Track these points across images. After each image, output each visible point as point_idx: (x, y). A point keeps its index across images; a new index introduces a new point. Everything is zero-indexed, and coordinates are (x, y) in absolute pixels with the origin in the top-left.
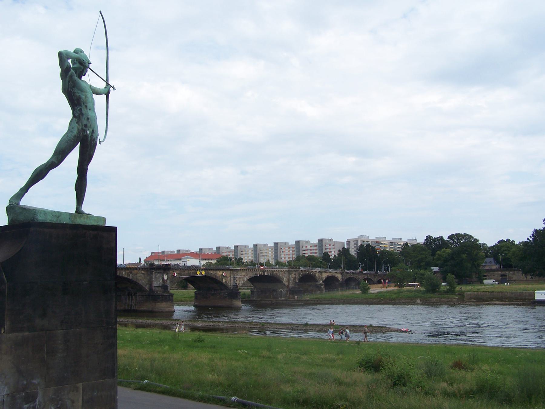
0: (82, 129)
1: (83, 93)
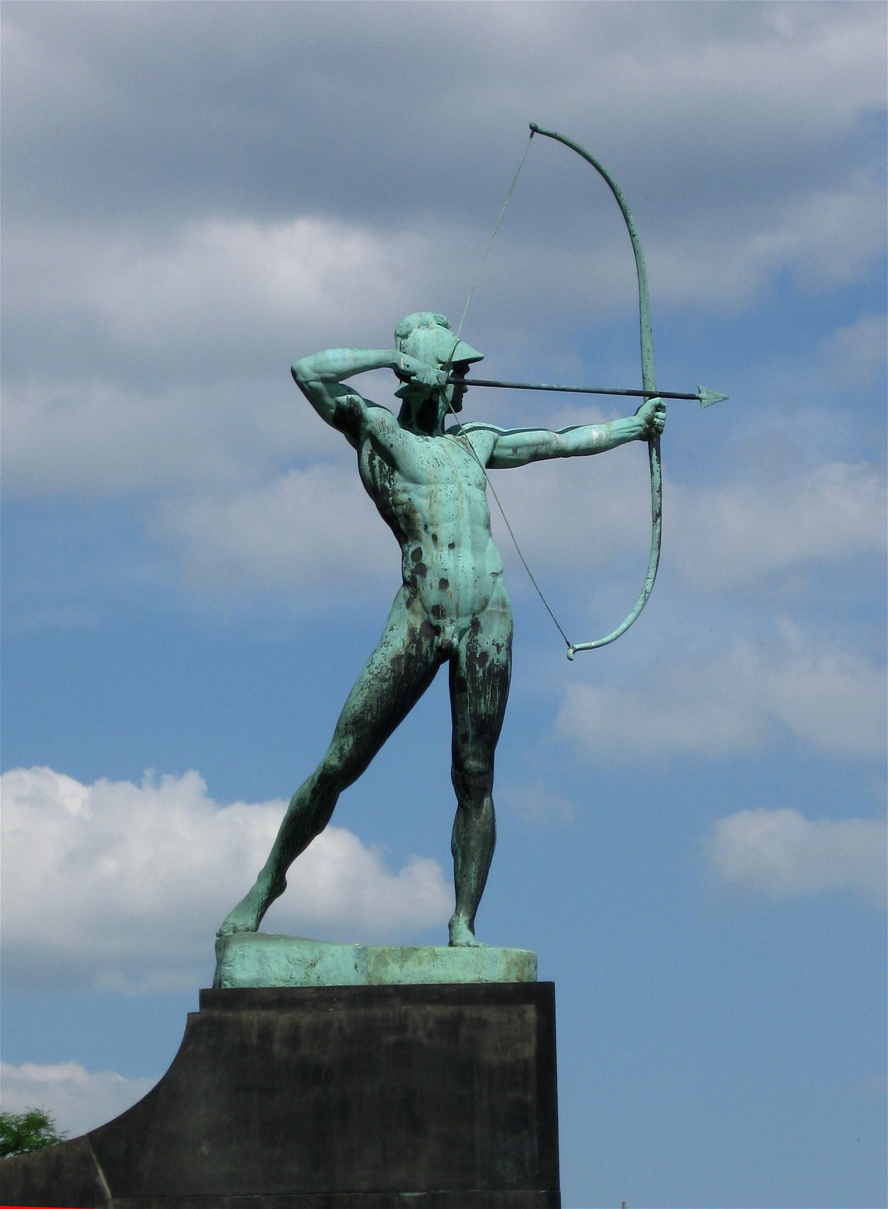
0: (427, 624)
1: (424, 489)
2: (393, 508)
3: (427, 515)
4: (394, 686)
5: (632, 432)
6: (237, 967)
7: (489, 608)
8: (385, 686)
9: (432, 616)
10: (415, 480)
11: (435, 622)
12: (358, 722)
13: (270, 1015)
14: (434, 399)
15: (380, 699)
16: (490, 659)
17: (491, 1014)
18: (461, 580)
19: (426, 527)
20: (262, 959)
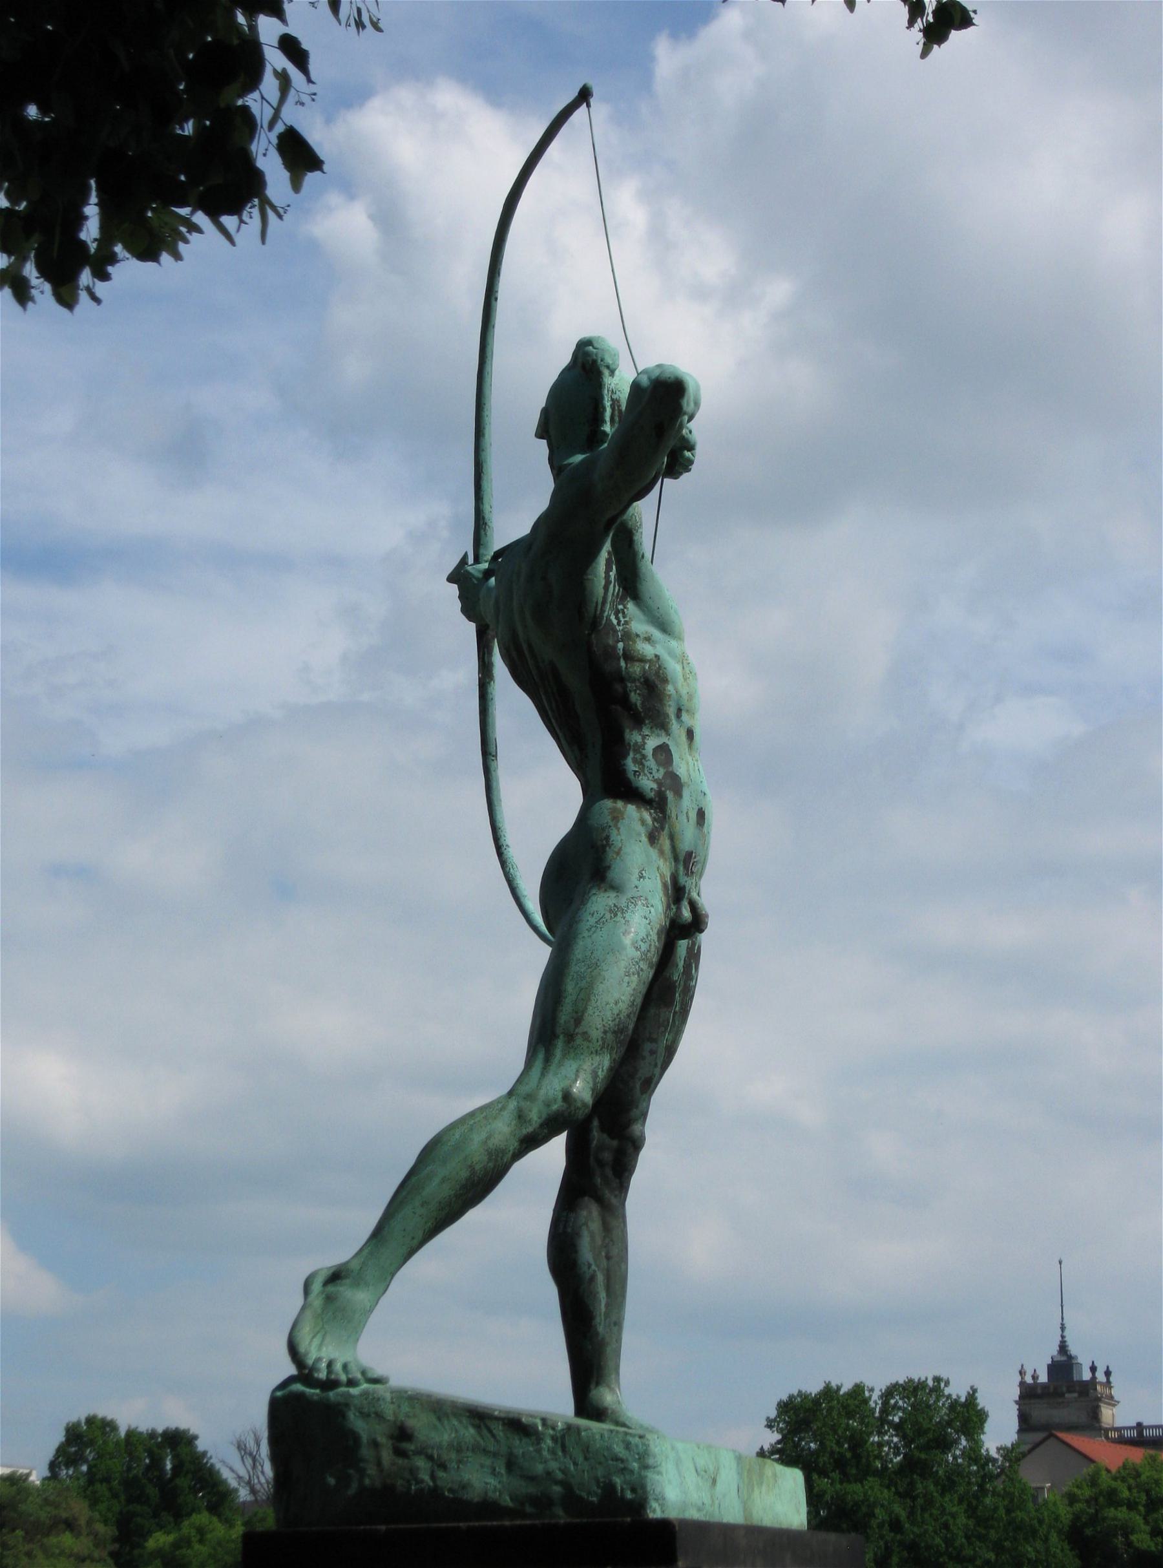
2: (623, 664)
3: (684, 692)
19: (679, 711)
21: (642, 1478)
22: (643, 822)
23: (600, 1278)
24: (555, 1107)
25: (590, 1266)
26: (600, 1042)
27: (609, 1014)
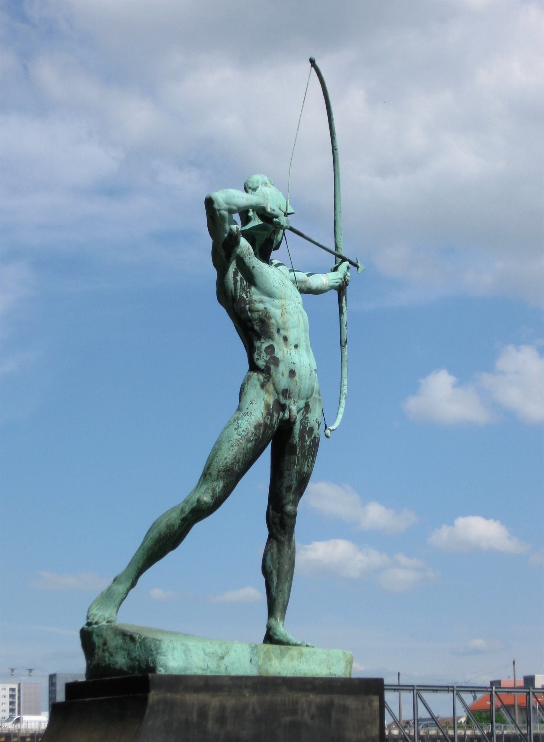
1: (277, 302)
2: (249, 314)
4: (255, 446)
5: (337, 282)
6: (170, 657)
7: (314, 395)
8: (250, 445)
9: (281, 397)
10: (270, 295)
11: (283, 401)
12: (229, 471)
13: (203, 697)
14: (272, 238)
15: (245, 455)
16: (315, 432)
17: (351, 702)
18: (303, 372)
19: (278, 331)
20: (186, 651)
21: (156, 658)
22: (259, 380)
23: (274, 572)
24: (194, 505)
25: (270, 567)
26: (216, 476)
27: (221, 464)
